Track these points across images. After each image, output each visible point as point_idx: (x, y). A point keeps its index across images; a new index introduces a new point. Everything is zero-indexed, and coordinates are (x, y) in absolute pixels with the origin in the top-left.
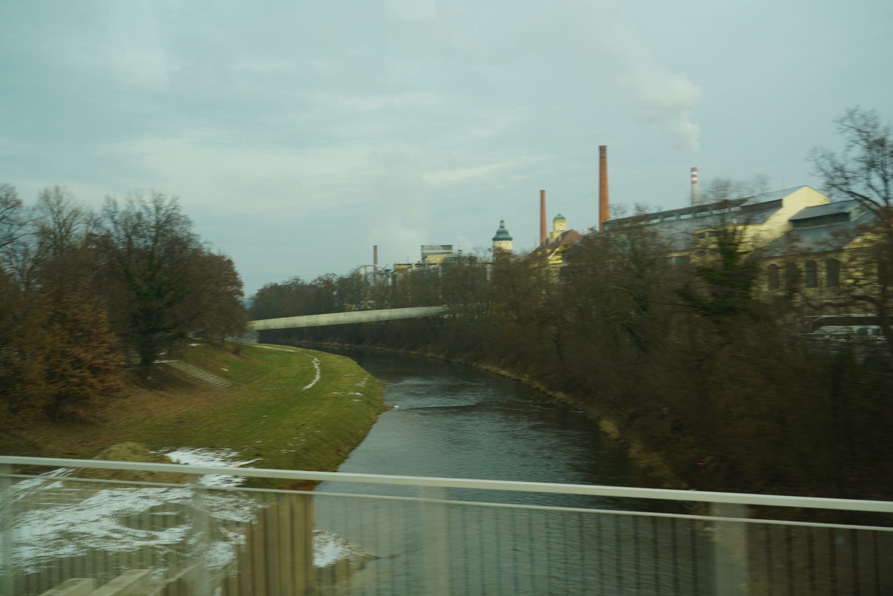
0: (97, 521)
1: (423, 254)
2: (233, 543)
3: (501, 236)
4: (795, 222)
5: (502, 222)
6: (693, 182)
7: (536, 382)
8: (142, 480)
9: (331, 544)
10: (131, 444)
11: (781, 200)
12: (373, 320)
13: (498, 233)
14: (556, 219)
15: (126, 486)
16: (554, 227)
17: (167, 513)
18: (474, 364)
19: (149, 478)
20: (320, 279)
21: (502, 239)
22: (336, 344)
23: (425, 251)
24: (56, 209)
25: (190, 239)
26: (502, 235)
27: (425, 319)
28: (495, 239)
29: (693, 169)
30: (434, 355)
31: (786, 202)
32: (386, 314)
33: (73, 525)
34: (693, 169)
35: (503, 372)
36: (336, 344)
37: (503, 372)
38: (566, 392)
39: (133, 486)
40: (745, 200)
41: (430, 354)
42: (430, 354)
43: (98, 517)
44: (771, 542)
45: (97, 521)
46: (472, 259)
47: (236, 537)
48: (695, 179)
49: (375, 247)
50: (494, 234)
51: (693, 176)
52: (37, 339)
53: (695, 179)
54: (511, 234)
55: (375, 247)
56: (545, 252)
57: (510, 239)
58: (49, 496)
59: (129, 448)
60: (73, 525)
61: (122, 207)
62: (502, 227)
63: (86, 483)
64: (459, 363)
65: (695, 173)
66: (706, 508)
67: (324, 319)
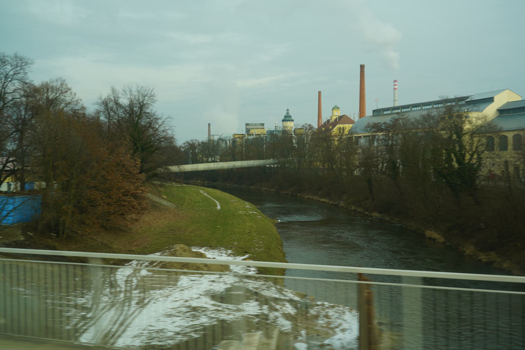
0: (198, 298)
1: (246, 129)
2: (281, 312)
3: (287, 119)
4: (501, 111)
5: (288, 110)
6: (395, 89)
7: (352, 206)
8: (202, 270)
9: (347, 313)
10: (182, 246)
11: (493, 97)
12: (231, 167)
13: (285, 117)
14: (333, 108)
15: (193, 274)
16: (333, 113)
17: (239, 293)
18: (299, 195)
19: (205, 268)
20: (187, 142)
21: (288, 121)
22: (199, 182)
23: (247, 127)
24: (142, 103)
25: (153, 120)
26: (287, 118)
27: (258, 167)
28: (283, 121)
29: (395, 81)
30: (267, 189)
31: (495, 99)
32: (238, 164)
33: (187, 301)
34: (395, 81)
35: (323, 200)
36: (199, 182)
37: (323, 200)
38: (380, 213)
39: (198, 273)
40: (468, 97)
41: (264, 189)
42: (264, 189)
43: (198, 296)
44: (435, 299)
45: (198, 298)
46: (322, 134)
47: (281, 308)
48: (396, 87)
49: (209, 125)
50: (283, 118)
51: (395, 85)
52: (86, 179)
53: (396, 87)
54: (293, 118)
55: (209, 125)
56: (329, 127)
57: (293, 121)
58: (152, 280)
59: (181, 248)
60: (187, 301)
61: (124, 101)
62: (287, 113)
63: (168, 272)
64: (288, 194)
65: (396, 83)
66: (398, 279)
67: (201, 167)
